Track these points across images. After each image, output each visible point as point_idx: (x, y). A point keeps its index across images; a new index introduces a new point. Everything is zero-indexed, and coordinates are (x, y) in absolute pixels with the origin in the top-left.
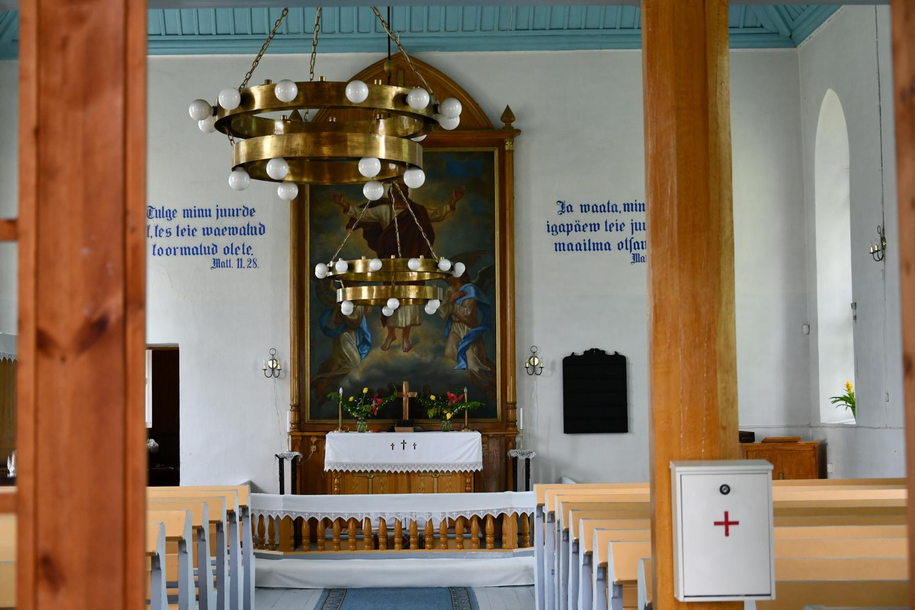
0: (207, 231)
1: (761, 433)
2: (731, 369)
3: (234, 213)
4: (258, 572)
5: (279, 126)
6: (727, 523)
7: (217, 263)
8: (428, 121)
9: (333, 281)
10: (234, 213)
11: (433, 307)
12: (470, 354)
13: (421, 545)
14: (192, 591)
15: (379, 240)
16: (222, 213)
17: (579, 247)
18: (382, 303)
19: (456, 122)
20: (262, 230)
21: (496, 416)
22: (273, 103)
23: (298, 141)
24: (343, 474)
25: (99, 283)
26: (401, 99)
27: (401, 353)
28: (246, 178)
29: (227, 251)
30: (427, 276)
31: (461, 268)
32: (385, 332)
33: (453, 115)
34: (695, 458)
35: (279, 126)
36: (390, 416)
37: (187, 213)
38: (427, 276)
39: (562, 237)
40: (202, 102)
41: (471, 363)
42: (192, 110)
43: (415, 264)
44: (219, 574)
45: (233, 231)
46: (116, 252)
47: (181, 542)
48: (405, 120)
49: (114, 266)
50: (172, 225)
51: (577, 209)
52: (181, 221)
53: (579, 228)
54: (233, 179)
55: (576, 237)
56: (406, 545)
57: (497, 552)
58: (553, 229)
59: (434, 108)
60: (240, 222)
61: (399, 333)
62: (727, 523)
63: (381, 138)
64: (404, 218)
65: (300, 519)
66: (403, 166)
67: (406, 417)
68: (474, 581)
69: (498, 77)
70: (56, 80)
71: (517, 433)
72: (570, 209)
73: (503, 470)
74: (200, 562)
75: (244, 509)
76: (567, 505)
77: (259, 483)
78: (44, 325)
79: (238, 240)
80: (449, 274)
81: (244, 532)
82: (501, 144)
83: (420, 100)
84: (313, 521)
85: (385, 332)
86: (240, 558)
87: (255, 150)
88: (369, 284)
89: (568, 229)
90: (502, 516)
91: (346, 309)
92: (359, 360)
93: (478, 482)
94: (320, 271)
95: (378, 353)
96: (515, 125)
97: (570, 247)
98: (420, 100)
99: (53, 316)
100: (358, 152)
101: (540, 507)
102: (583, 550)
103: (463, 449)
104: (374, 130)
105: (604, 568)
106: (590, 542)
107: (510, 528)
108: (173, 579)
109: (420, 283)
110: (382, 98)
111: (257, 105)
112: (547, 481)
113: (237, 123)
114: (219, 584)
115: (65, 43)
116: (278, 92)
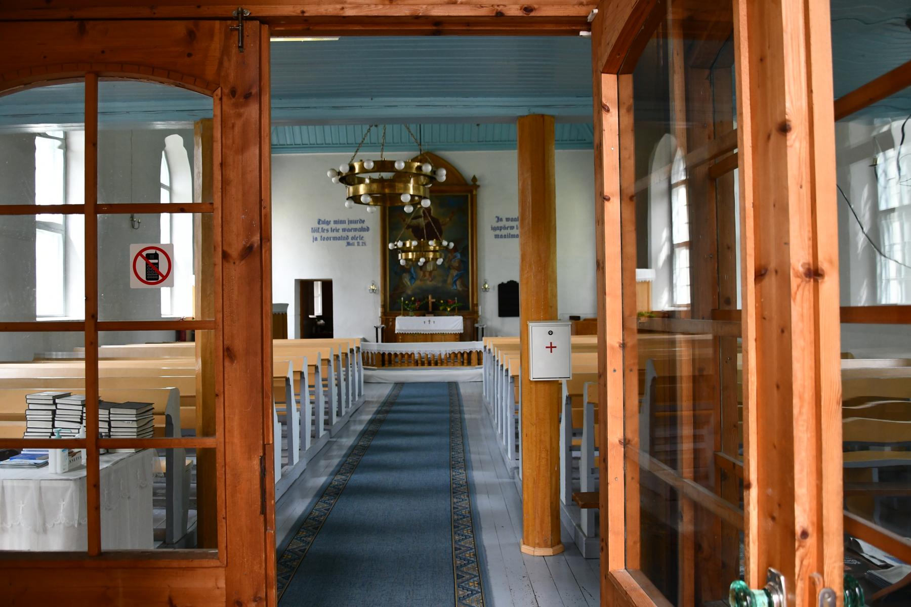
0: (344, 230)
1: (583, 316)
2: (554, 282)
3: (355, 222)
4: (365, 376)
5: (367, 181)
6: (551, 347)
7: (348, 244)
8: (432, 178)
9: (396, 251)
10: (355, 222)
11: (440, 261)
12: (458, 283)
13: (436, 364)
14: (334, 382)
15: (417, 233)
16: (351, 222)
17: (505, 236)
18: (418, 260)
19: (444, 178)
20: (368, 229)
21: (468, 308)
22: (363, 170)
23: (375, 186)
24: (403, 335)
25: (249, 231)
26: (419, 168)
27: (429, 283)
28: (353, 203)
29: (353, 238)
30: (437, 248)
31: (452, 245)
32: (421, 273)
33: (443, 175)
34: (538, 320)
35: (367, 181)
36: (424, 310)
37: (336, 222)
38: (437, 248)
39: (498, 232)
40: (333, 170)
41: (459, 287)
42: (329, 174)
43: (432, 243)
44: (347, 375)
45: (355, 230)
46: (257, 217)
47: (329, 361)
48: (422, 178)
49: (256, 223)
50: (329, 227)
51: (504, 220)
52: (332, 225)
53: (505, 228)
54: (347, 204)
55: (504, 232)
56: (429, 364)
57: (468, 367)
58: (494, 229)
59: (434, 172)
60: (358, 226)
61: (427, 274)
62: (551, 347)
63: (411, 186)
64: (428, 225)
65: (384, 354)
66: (421, 198)
67: (430, 309)
68: (459, 379)
69: (470, 162)
70: (230, 142)
71: (478, 316)
72: (501, 220)
73: (472, 333)
74: (337, 370)
75: (358, 348)
76: (495, 345)
77: (367, 338)
78: (225, 248)
79: (357, 234)
80: (447, 247)
81: (358, 358)
82: (471, 192)
83: (427, 168)
84: (390, 354)
85: (421, 273)
86: (356, 369)
87: (356, 190)
88: (412, 252)
89: (500, 229)
90: (471, 352)
91: (402, 262)
92: (410, 285)
93: (461, 337)
94: (390, 246)
95: (418, 283)
96: (478, 183)
97: (501, 236)
98: (427, 168)
99: (230, 245)
100: (401, 191)
101: (485, 347)
102: (500, 364)
103: (454, 323)
104: (409, 182)
105: (507, 370)
106: (502, 360)
107: (474, 358)
108: (325, 377)
109: (434, 251)
110: (411, 168)
111: (357, 171)
112: (491, 336)
113: (348, 179)
114: (346, 380)
115: (233, 126)
116: (365, 165)
